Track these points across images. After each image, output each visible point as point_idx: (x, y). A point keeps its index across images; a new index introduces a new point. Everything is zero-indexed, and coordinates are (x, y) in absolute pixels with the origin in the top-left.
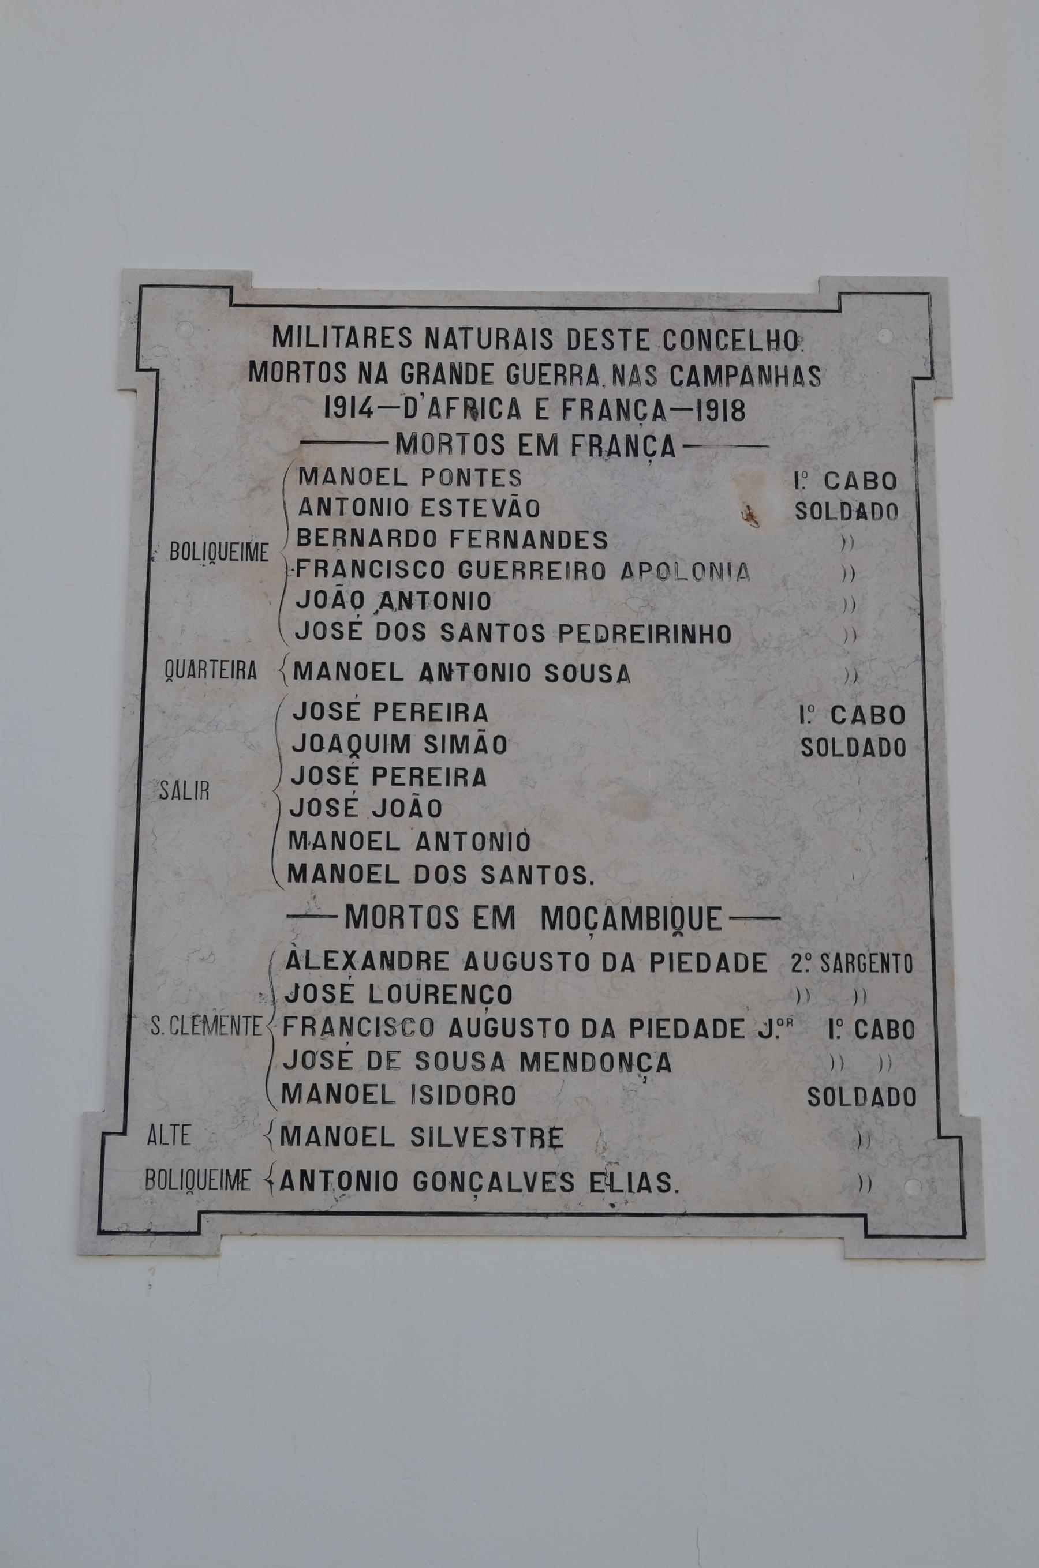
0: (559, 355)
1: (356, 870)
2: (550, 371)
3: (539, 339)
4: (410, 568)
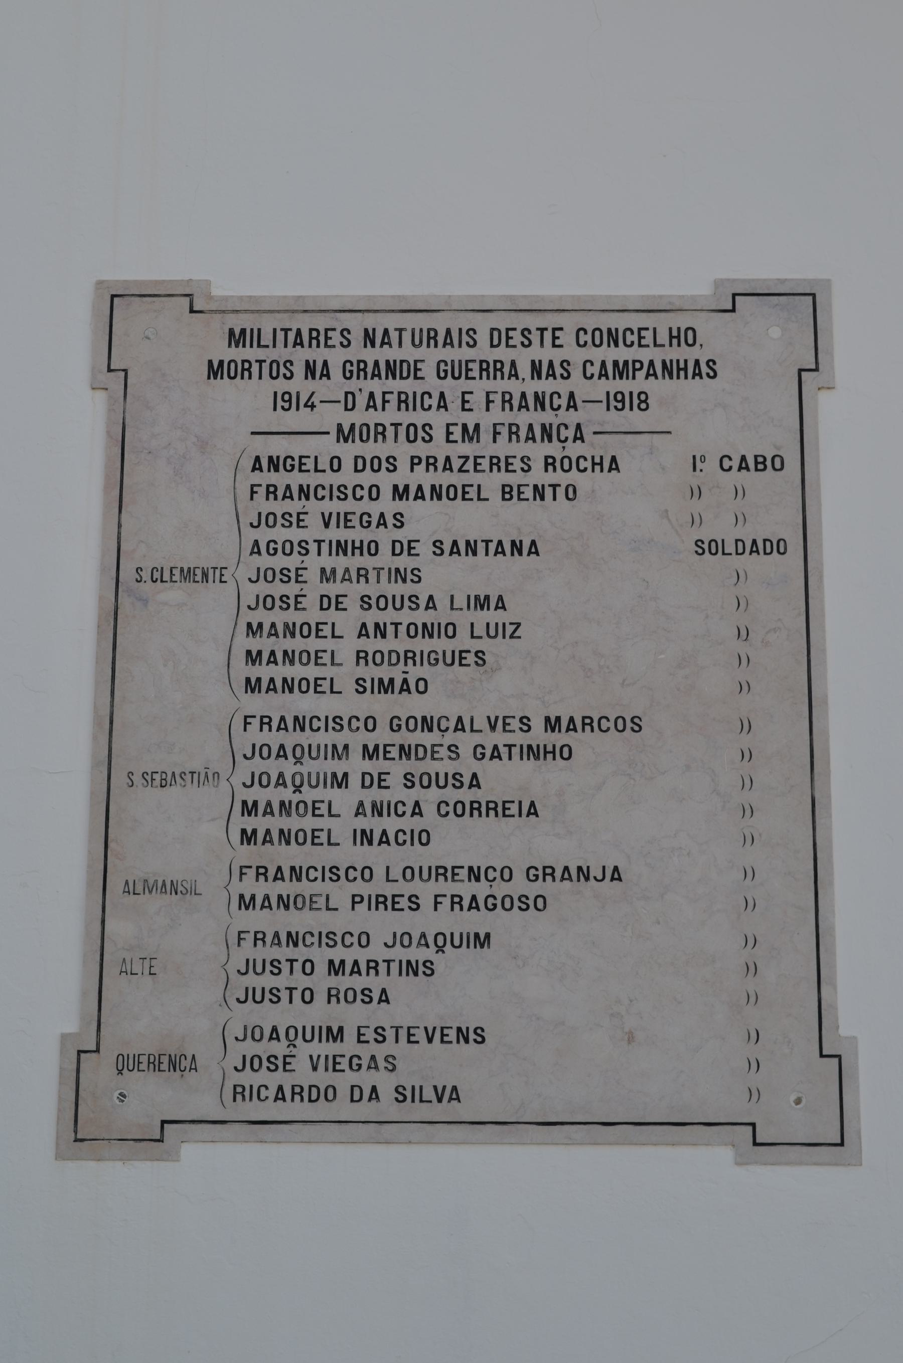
0: (484, 351)
1: (305, 633)
2: (475, 367)
3: (465, 338)
4: (349, 492)
